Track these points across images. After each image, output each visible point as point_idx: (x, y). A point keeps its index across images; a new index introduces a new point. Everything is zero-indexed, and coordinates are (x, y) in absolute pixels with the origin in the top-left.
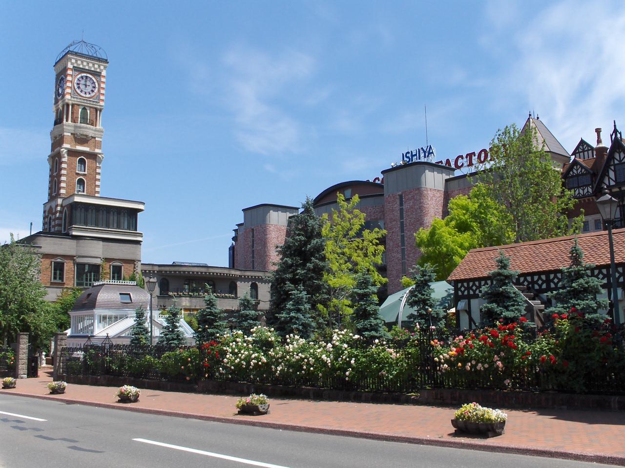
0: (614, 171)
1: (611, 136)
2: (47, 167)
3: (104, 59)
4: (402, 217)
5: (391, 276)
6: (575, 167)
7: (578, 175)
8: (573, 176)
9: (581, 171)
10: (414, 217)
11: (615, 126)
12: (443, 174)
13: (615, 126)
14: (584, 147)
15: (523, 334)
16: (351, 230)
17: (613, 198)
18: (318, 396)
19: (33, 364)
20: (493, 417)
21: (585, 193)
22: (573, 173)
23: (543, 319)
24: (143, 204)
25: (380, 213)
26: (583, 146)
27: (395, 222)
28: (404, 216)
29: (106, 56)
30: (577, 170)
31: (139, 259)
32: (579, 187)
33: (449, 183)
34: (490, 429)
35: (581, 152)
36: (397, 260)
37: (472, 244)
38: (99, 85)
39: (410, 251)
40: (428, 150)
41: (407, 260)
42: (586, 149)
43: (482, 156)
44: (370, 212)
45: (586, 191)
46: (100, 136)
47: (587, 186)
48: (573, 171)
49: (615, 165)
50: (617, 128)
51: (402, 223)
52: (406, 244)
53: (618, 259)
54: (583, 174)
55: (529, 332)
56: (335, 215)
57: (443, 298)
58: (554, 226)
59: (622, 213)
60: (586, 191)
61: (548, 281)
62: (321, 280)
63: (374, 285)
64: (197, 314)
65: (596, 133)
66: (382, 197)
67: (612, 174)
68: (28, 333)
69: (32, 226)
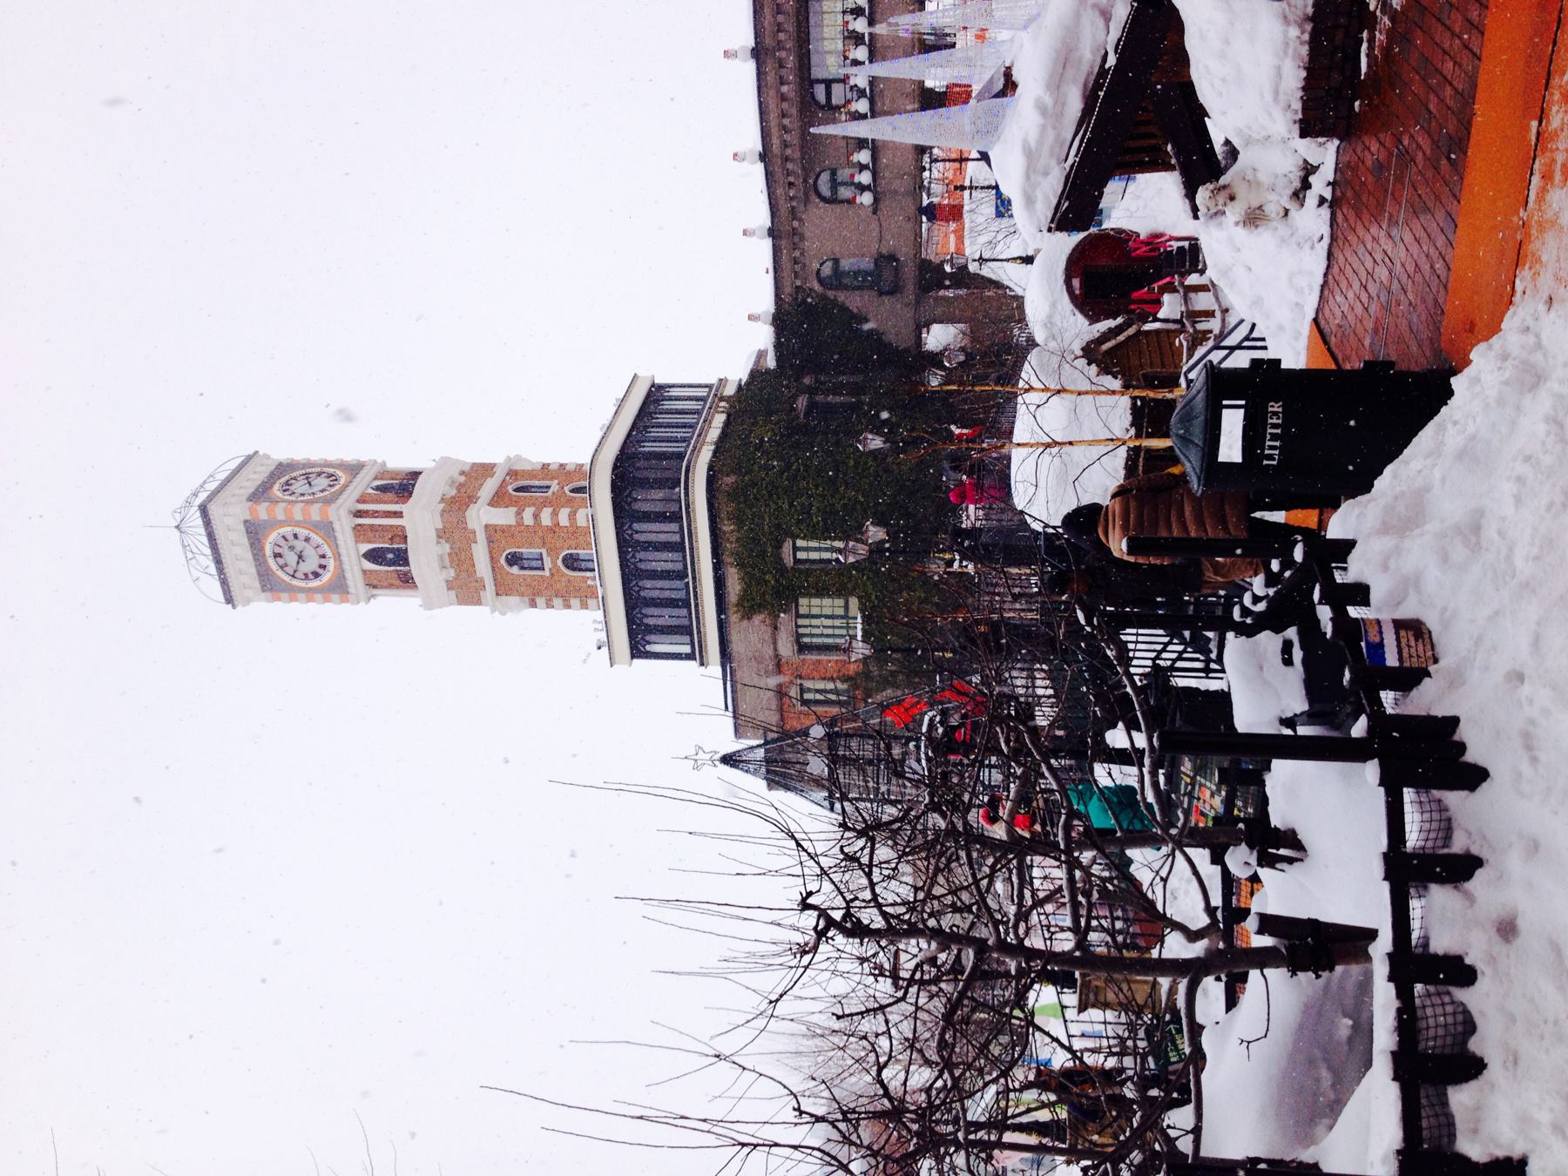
2: (1194, 878)
12: (825, 8)
17: (1192, 607)
18: (634, 426)
19: (390, 556)
20: (738, 588)
23: (1120, 320)
24: (1524, 247)
31: (878, 16)
34: (1288, 662)
35: (1033, 683)
38: (282, 524)
43: (1149, 392)
55: (783, 474)
57: (1021, 307)
58: (908, 676)
59: (819, 697)
61: (804, 32)
62: (863, 35)
64: (1150, 1070)
65: (1386, 886)
66: (951, 50)
68: (1243, 402)
69: (782, 1143)
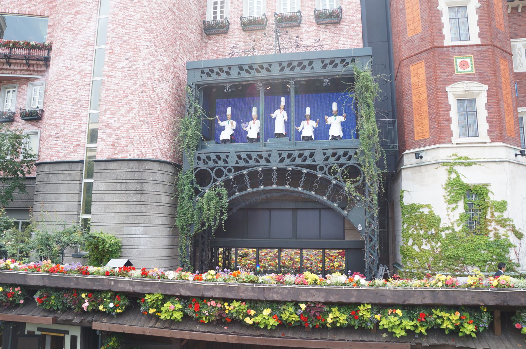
5: (57, 115)
36: (78, 77)
41: (108, 77)
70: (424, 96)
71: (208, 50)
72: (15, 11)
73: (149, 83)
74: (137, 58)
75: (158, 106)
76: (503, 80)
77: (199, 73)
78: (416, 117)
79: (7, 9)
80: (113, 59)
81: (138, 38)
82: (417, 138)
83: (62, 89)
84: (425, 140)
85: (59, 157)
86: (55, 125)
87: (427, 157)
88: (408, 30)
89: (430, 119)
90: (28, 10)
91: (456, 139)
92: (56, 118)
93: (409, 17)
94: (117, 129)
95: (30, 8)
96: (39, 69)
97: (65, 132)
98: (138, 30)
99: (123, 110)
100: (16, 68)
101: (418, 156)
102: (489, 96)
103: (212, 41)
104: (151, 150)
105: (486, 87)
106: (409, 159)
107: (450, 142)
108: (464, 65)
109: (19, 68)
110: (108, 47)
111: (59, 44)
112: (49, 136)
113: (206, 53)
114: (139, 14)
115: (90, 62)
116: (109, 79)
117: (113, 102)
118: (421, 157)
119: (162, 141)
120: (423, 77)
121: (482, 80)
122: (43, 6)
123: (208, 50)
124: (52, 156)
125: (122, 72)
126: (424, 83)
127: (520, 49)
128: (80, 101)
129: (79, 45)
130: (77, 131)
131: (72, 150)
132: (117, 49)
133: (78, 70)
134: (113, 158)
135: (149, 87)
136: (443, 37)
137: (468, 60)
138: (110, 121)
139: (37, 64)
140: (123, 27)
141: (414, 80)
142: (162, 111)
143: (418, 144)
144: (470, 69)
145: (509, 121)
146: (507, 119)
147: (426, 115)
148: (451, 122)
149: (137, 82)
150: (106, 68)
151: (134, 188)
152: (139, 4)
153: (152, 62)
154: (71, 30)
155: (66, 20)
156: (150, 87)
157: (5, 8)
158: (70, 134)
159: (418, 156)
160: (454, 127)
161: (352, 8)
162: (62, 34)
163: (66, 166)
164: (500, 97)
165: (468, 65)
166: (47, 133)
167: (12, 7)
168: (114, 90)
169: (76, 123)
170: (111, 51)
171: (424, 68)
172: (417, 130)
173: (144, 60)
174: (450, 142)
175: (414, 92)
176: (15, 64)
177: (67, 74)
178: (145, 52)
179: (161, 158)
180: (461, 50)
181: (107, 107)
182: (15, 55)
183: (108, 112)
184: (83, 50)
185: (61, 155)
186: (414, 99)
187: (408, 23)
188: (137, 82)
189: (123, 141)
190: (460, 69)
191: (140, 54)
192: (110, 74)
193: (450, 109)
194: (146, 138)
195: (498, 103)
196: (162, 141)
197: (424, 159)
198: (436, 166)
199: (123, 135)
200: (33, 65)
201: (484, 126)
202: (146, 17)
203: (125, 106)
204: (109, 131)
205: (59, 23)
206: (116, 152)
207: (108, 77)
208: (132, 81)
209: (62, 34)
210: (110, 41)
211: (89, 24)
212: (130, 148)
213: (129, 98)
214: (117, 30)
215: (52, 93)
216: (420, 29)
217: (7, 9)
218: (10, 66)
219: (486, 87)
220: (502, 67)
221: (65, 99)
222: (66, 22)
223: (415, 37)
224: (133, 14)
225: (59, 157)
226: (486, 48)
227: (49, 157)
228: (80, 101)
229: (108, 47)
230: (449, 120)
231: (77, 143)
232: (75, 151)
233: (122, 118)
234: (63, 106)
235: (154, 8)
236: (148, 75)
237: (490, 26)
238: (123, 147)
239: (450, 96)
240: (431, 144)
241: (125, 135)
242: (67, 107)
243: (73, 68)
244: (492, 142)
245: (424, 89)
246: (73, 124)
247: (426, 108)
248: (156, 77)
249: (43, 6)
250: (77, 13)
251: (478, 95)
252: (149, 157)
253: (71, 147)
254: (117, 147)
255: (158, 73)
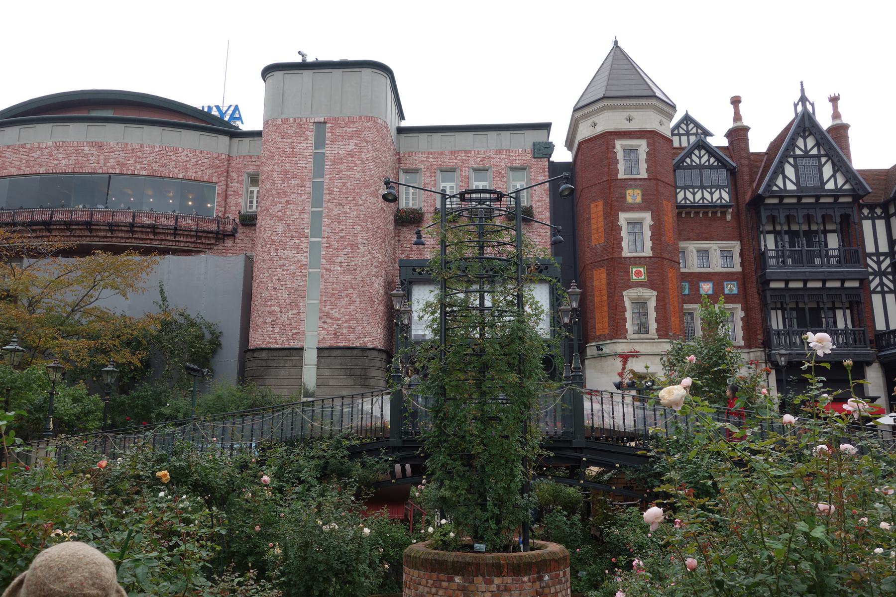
0: (795, 166)
1: (796, 105)
3: (211, 232)
4: (319, 170)
5: (272, 302)
6: (696, 152)
7: (701, 167)
8: (690, 168)
9: (708, 160)
10: (358, 175)
11: (803, 90)
13: (803, 90)
14: (690, 129)
15: (628, 445)
16: (307, 444)
21: (714, 200)
22: (692, 161)
25: (209, 168)
26: (687, 125)
27: (298, 182)
28: (327, 172)
29: (542, 186)
30: (700, 158)
32: (702, 187)
33: (403, 136)
36: (293, 267)
37: (300, 547)
39: (337, 250)
40: (230, 112)
41: (326, 270)
42: (694, 131)
44: (186, 161)
45: (716, 196)
46: (857, 339)
47: (719, 187)
48: (691, 158)
49: (796, 157)
50: (807, 94)
51: (318, 188)
52: (326, 231)
53: (892, 328)
54: (711, 167)
56: (387, 515)
60: (716, 196)
63: (291, 247)
67: (790, 171)
70: (605, 298)
71: (402, 238)
72: (181, 176)
73: (368, 279)
74: (355, 255)
75: (376, 300)
76: (670, 285)
77: (410, 271)
78: (598, 315)
79: (172, 173)
80: (331, 253)
81: (356, 235)
82: (598, 333)
83: (276, 277)
84: (605, 335)
85: (277, 344)
86: (271, 313)
87: (607, 350)
88: (593, 238)
89: (609, 318)
90: (194, 175)
91: (630, 334)
92: (271, 306)
93: (594, 227)
94: (339, 319)
95: (196, 173)
96: (207, 242)
97: (282, 319)
98: (355, 227)
99: (344, 302)
100: (182, 239)
101: (599, 348)
102: (657, 301)
103: (405, 229)
104: (371, 339)
105: (655, 293)
106: (591, 350)
107: (625, 338)
108: (638, 273)
109: (185, 240)
110: (325, 240)
111: (270, 232)
112: (264, 323)
113: (399, 241)
114: (355, 212)
115: (305, 254)
116: (328, 273)
117: (333, 294)
118: (602, 350)
119: (379, 331)
120: (604, 282)
121: (652, 288)
122: (210, 171)
123: (402, 238)
124: (269, 342)
125: (341, 266)
126: (605, 287)
127: (692, 251)
128: (297, 290)
129: (292, 236)
130: (295, 319)
131: (291, 337)
132: (335, 244)
133: (292, 260)
134: (335, 345)
135: (368, 282)
136: (622, 249)
137: (642, 270)
138: (331, 312)
139: (206, 237)
140: (339, 223)
141: (596, 283)
142: (379, 304)
143: (599, 338)
144: (643, 277)
145: (674, 320)
146: (673, 319)
147: (606, 314)
148: (626, 322)
149: (357, 277)
150: (324, 261)
151: (358, 373)
152: (354, 202)
153: (369, 259)
154: (282, 220)
155: (276, 208)
156: (368, 282)
157: (169, 172)
158: (288, 322)
159: (599, 348)
160: (629, 325)
161: (542, 206)
162: (272, 222)
163: (286, 352)
164: (667, 301)
165: (641, 273)
166: (261, 320)
167: (176, 171)
168: (333, 283)
169: (294, 312)
170: (328, 245)
171: (605, 274)
172: (598, 326)
173: (363, 257)
174: (625, 338)
175: (596, 293)
176: (180, 235)
177: (281, 263)
178: (363, 249)
179: (379, 347)
180: (637, 261)
181: (327, 299)
182: (181, 227)
183: (328, 303)
184: (297, 241)
185: (279, 342)
186: (597, 300)
187: (593, 232)
188: (357, 277)
189: (345, 331)
190: (634, 277)
191: (358, 251)
192: (328, 267)
193: (625, 310)
194: (367, 329)
195: (664, 306)
196: (379, 331)
197: (604, 351)
198: (613, 357)
199: (345, 325)
200: (201, 237)
201: (653, 326)
202: (362, 216)
203: (345, 299)
204: (330, 321)
205: (268, 211)
206: (339, 341)
207: (326, 270)
208: (351, 276)
209: (272, 222)
210: (326, 236)
211: (302, 216)
212: (352, 337)
213: (349, 292)
214: (333, 225)
215: (265, 280)
216: (602, 240)
217: (172, 173)
218: (175, 237)
219: (655, 293)
220: (670, 275)
221: (281, 288)
222: (276, 210)
223: (599, 246)
224: (348, 211)
225: (277, 344)
226: (657, 260)
227: (265, 343)
228: (297, 290)
229: (325, 240)
230: (625, 320)
231: (297, 331)
232: (294, 339)
233: (343, 310)
234: (279, 295)
235: (369, 208)
236: (366, 272)
237: (660, 241)
238: (345, 336)
239: (626, 299)
240: (610, 339)
241: (346, 325)
242: (283, 295)
243: (287, 258)
244: (659, 338)
245: (605, 292)
246: (290, 313)
247: (606, 308)
248: (373, 273)
249: (210, 171)
250: (288, 202)
251: (648, 299)
252: (370, 346)
253: (290, 334)
254: (339, 336)
255: (375, 270)
